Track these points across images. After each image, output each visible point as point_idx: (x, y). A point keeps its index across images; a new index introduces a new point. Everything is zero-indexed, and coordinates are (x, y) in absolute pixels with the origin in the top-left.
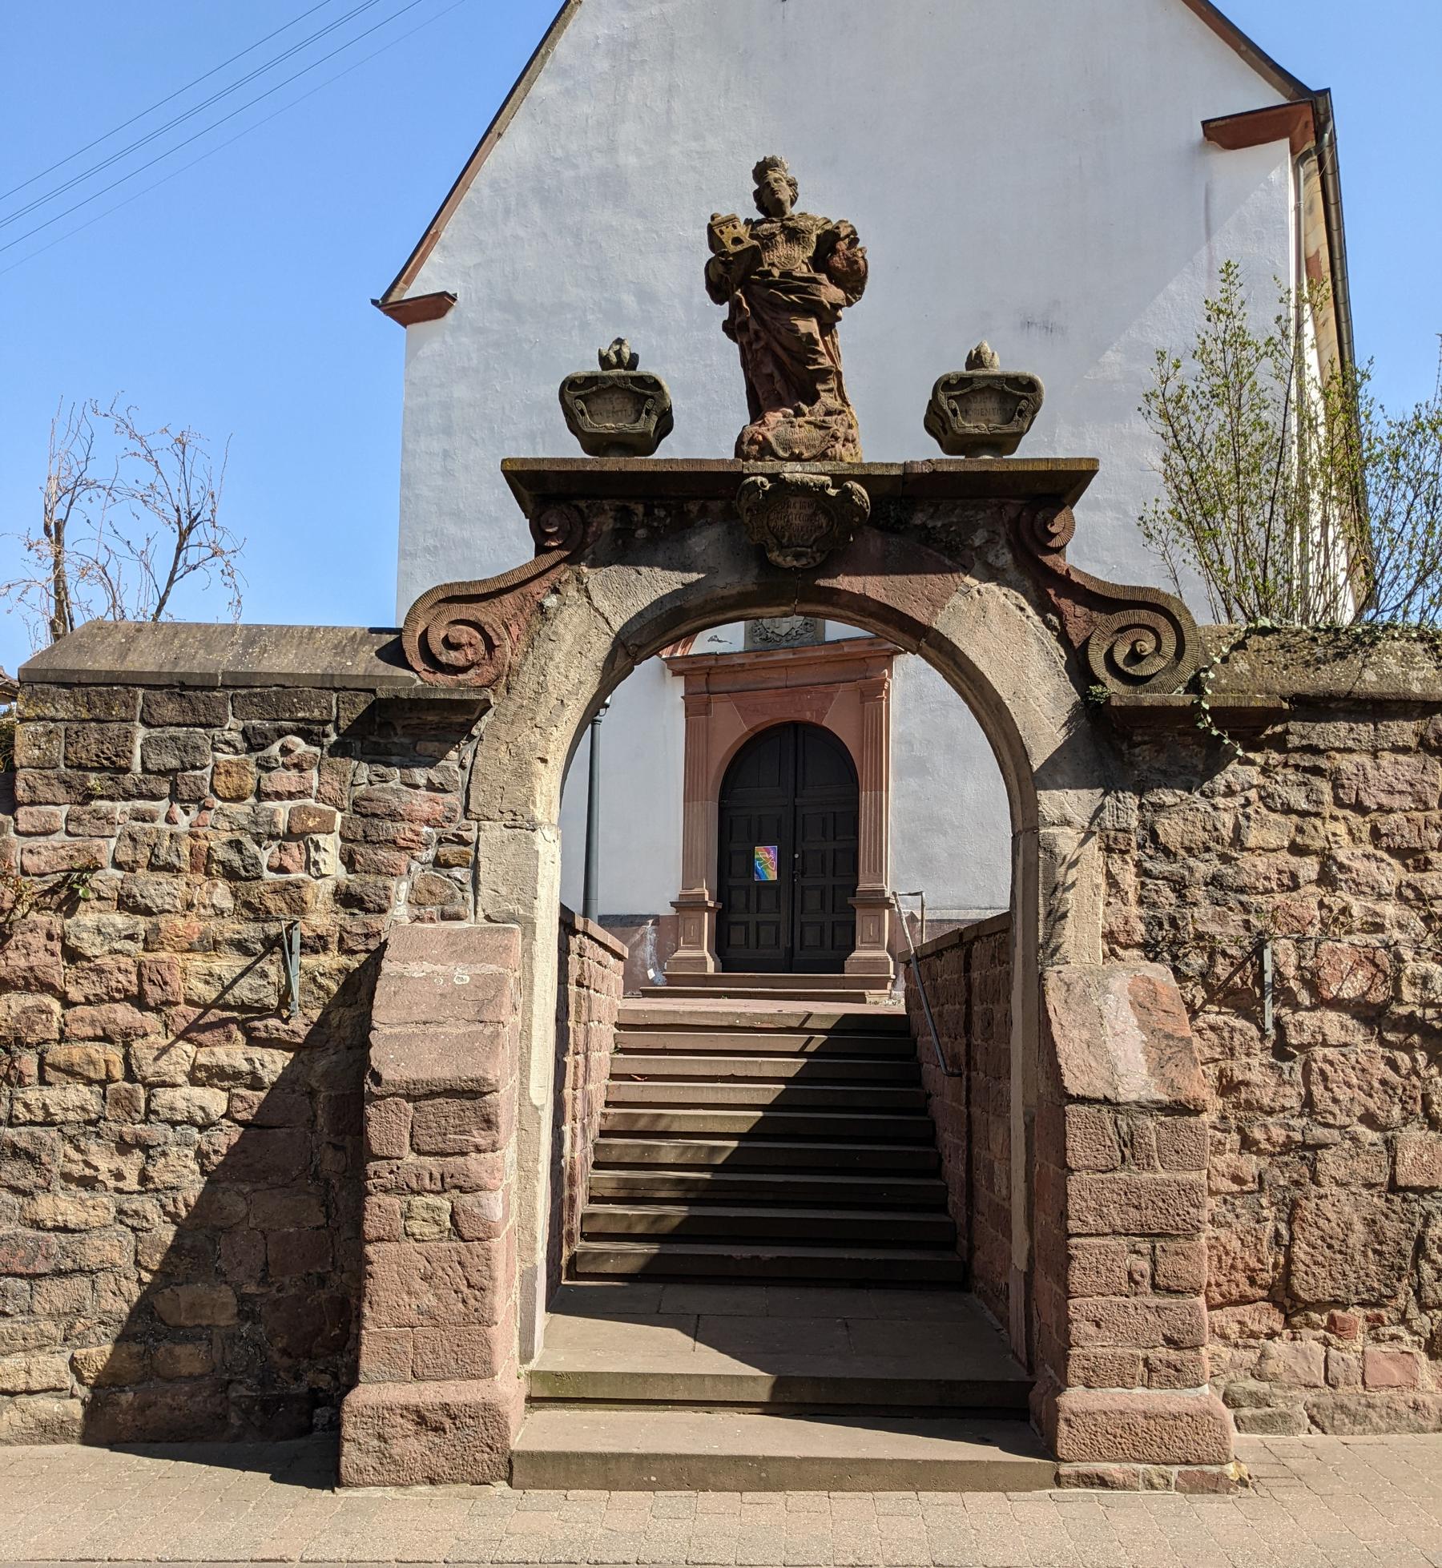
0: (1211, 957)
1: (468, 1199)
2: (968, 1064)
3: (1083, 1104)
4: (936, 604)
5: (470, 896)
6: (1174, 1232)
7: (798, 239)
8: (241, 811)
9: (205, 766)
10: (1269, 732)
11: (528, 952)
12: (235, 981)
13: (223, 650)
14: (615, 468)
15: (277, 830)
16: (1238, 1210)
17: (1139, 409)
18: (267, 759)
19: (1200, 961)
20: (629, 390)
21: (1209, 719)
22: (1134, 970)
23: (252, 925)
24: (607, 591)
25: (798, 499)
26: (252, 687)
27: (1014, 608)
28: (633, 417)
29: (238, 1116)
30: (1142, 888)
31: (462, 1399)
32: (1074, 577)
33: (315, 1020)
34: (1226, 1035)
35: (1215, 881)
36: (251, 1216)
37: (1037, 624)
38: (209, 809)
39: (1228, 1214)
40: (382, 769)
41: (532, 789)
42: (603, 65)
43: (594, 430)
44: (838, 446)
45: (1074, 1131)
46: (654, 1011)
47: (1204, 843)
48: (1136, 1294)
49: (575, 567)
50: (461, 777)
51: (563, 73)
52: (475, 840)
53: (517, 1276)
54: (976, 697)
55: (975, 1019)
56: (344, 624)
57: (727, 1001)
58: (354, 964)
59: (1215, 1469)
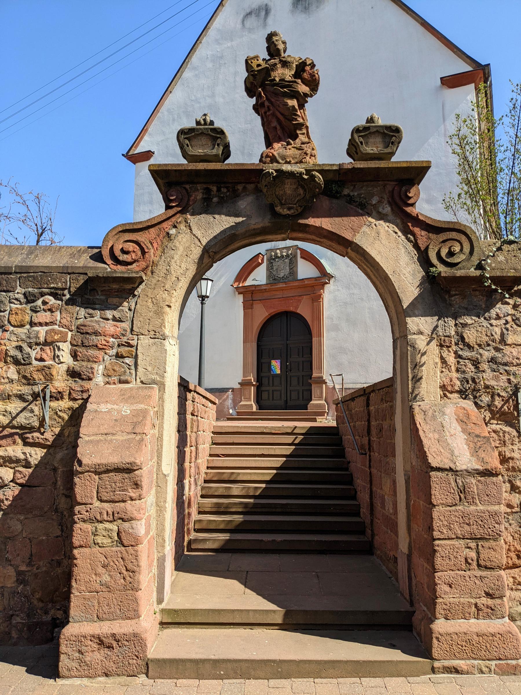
0: (492, 397)
1: (126, 525)
2: (369, 449)
3: (439, 471)
4: (355, 231)
5: (133, 372)
6: (488, 537)
7: (287, 66)
8: (22, 332)
9: (5, 311)
10: (516, 289)
11: (161, 398)
12: (18, 414)
13: (17, 256)
14: (203, 168)
15: (39, 341)
16: (511, 521)
17: (447, 142)
18: (35, 307)
19: (487, 399)
20: (209, 135)
21: (490, 282)
22: (456, 404)
23: (27, 387)
24: (199, 227)
25: (289, 180)
26: (29, 273)
27: (392, 232)
28: (211, 147)
29: (18, 481)
30: (458, 364)
31: (122, 631)
32: (420, 217)
33: (57, 433)
34: (501, 434)
35: (493, 360)
36: (24, 531)
37: (403, 239)
38: (7, 331)
39: (506, 524)
40: (91, 311)
41: (163, 320)
42: (210, 65)
43: (193, 153)
44: (308, 158)
45: (435, 485)
46: (229, 426)
47: (487, 342)
48: (469, 570)
49: (184, 215)
50: (129, 314)
51: (195, 68)
52: (136, 344)
53: (156, 560)
54: (374, 275)
55: (372, 428)
56: (76, 245)
57: (261, 422)
58: (76, 405)
59: (514, 662)
